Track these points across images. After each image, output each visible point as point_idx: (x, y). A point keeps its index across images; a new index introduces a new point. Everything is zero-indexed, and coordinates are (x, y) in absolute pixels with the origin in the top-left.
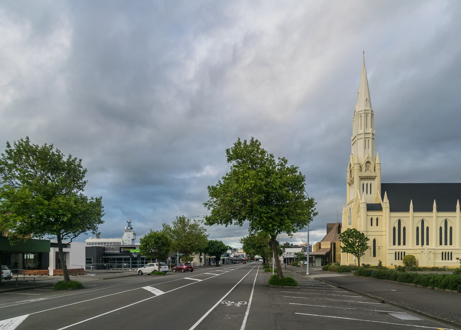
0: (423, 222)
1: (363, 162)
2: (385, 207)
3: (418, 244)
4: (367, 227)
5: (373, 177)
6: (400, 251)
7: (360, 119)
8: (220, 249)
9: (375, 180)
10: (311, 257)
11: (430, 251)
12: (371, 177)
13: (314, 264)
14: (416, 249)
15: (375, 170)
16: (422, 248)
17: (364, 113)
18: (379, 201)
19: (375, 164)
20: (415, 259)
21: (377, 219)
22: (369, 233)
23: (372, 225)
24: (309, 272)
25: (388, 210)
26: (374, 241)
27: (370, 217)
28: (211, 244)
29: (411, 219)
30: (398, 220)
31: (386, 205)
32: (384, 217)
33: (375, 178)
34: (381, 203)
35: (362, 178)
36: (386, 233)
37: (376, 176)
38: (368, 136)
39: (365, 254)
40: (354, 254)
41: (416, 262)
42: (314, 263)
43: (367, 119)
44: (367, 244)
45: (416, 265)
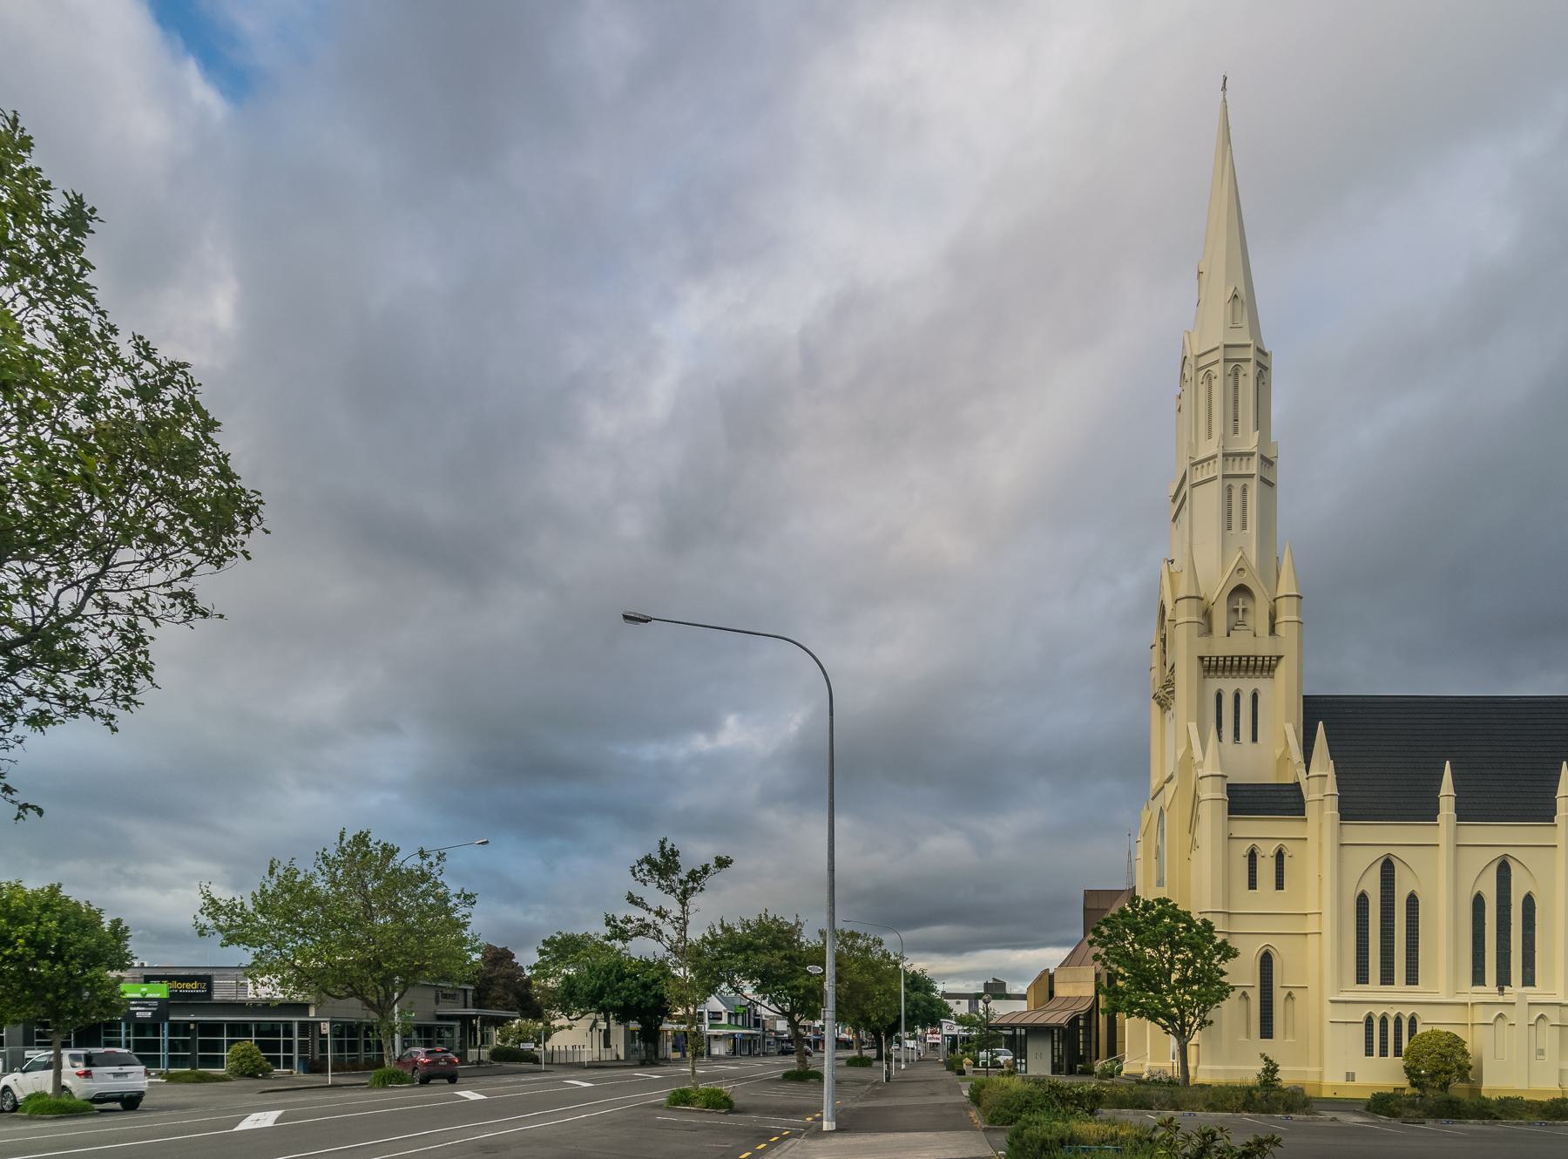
0: (1504, 871)
1: (1215, 586)
2: (1317, 796)
3: (1478, 978)
4: (1228, 896)
5: (1267, 663)
6: (1393, 1014)
7: (1203, 389)
8: (654, 992)
9: (1273, 677)
10: (1010, 1033)
11: (1542, 1016)
14: (1472, 1004)
15: (1272, 631)
16: (1501, 999)
17: (1222, 361)
18: (1294, 773)
19: (1275, 600)
20: (1465, 1053)
21: (1280, 856)
22: (1240, 925)
23: (1252, 884)
24: (837, 1118)
25: (1331, 810)
26: (1266, 960)
27: (1245, 847)
28: (617, 972)
29: (1443, 856)
30: (1383, 859)
31: (1322, 788)
32: (1312, 844)
33: (1276, 666)
34: (1299, 783)
35: (1211, 667)
36: (1320, 920)
37: (1279, 658)
38: (1241, 469)
39: (1211, 1022)
40: (1164, 1022)
41: (1470, 1068)
42: (1023, 1061)
43: (1236, 387)
44: (1223, 973)
45: (1468, 1081)
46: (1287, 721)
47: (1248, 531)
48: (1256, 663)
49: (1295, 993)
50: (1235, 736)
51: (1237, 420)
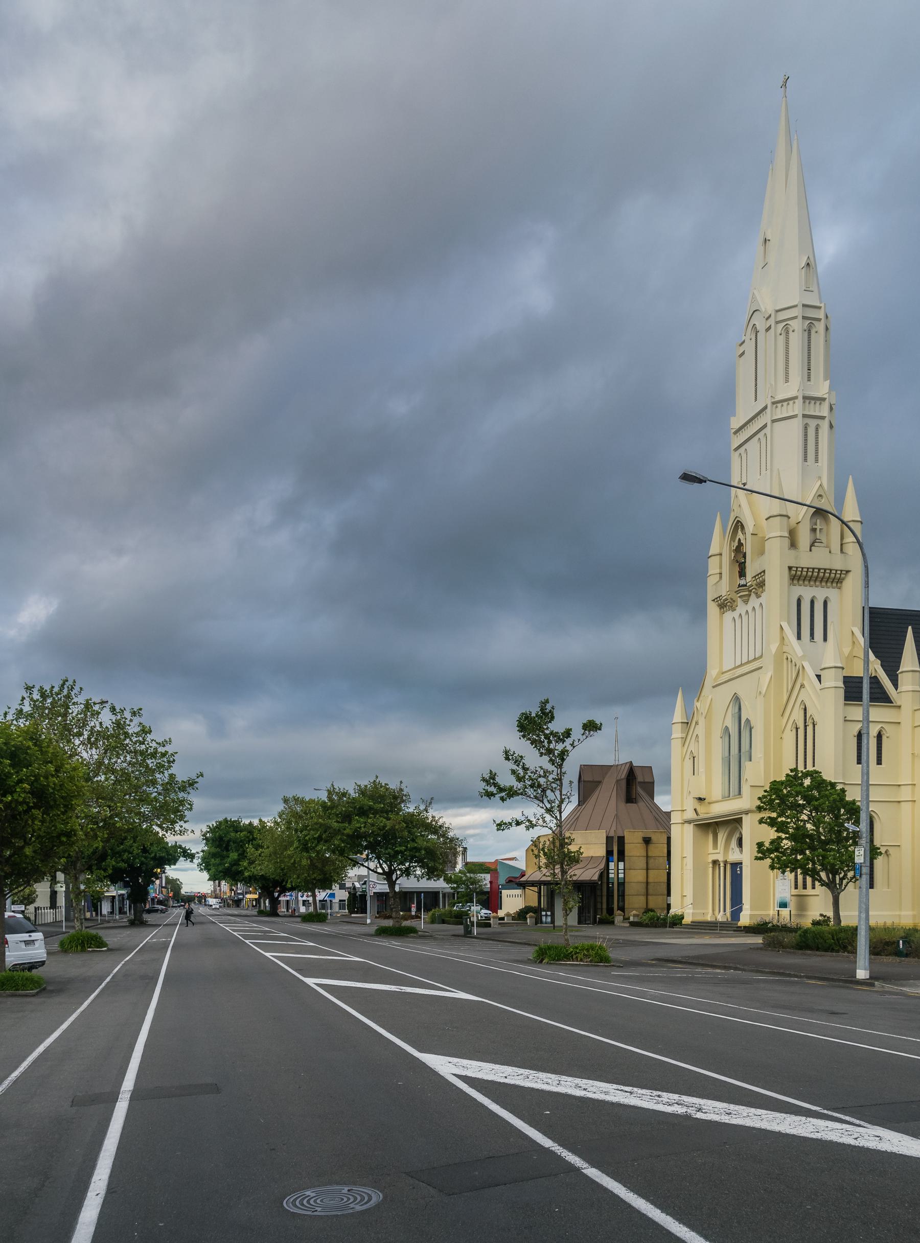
7: (781, 339)
8: (153, 855)
12: (818, 573)
13: (546, 915)
33: (844, 579)
35: (798, 576)
37: (848, 572)
42: (549, 913)
46: (853, 626)
47: (819, 464)
48: (818, 575)
49: (891, 850)
50: (811, 636)
51: (810, 370)
